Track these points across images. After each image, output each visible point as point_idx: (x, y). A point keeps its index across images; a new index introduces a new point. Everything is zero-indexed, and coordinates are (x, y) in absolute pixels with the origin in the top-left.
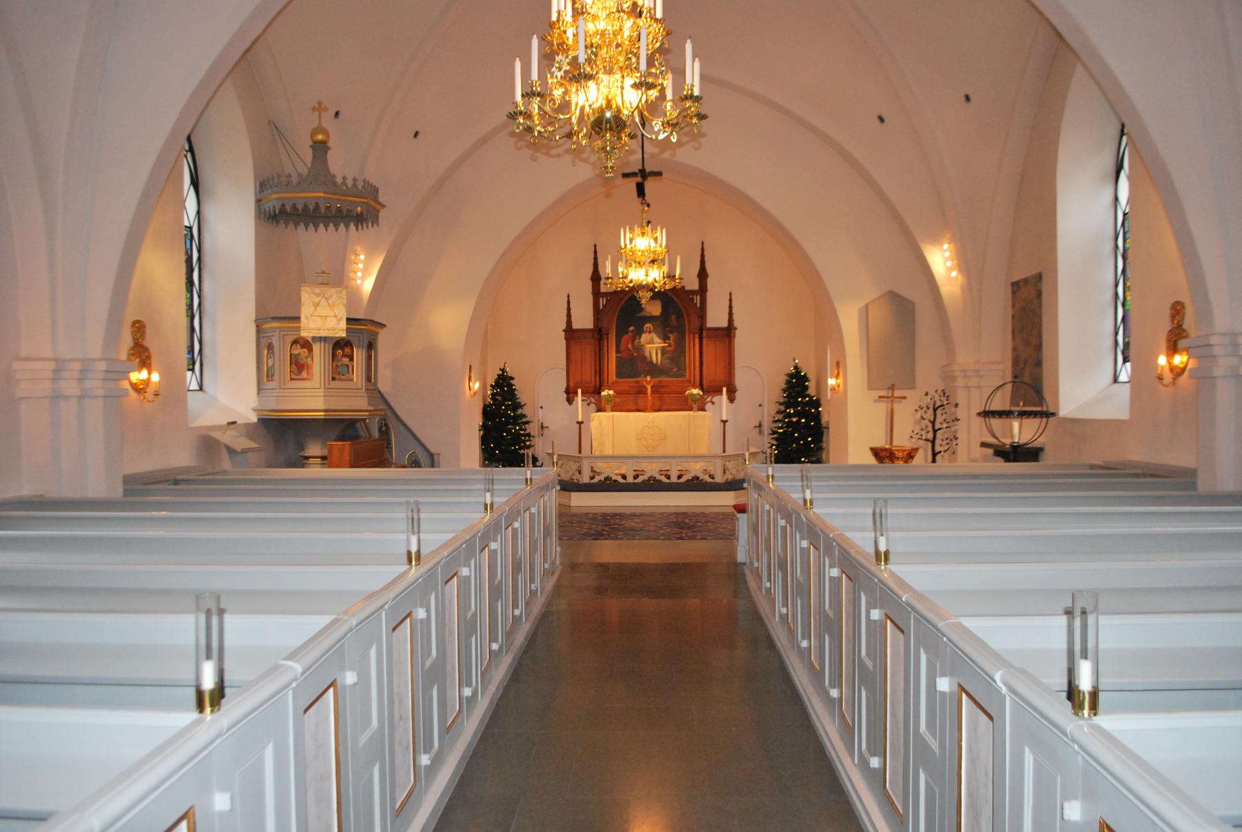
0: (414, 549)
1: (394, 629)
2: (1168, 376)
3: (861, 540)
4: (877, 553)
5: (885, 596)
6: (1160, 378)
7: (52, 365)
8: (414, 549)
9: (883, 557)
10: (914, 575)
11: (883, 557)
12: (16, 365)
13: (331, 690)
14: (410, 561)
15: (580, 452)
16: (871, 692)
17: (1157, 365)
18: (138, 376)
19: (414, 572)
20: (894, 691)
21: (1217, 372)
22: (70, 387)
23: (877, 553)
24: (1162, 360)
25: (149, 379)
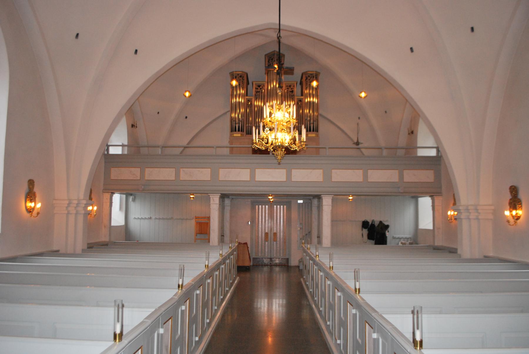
0: (180, 283)
1: (164, 324)
2: (512, 221)
3: (351, 284)
4: (356, 289)
5: (358, 306)
6: (508, 221)
7: (67, 202)
8: (180, 283)
9: (358, 291)
10: (370, 299)
11: (358, 291)
12: (54, 202)
13: (140, 350)
14: (115, 338)
15: (330, 148)
16: (344, 329)
17: (42, 205)
18: (30, 205)
19: (120, 345)
20: (350, 329)
21: (462, 217)
22: (72, 210)
23: (356, 289)
24: (507, 213)
25: (511, 212)
